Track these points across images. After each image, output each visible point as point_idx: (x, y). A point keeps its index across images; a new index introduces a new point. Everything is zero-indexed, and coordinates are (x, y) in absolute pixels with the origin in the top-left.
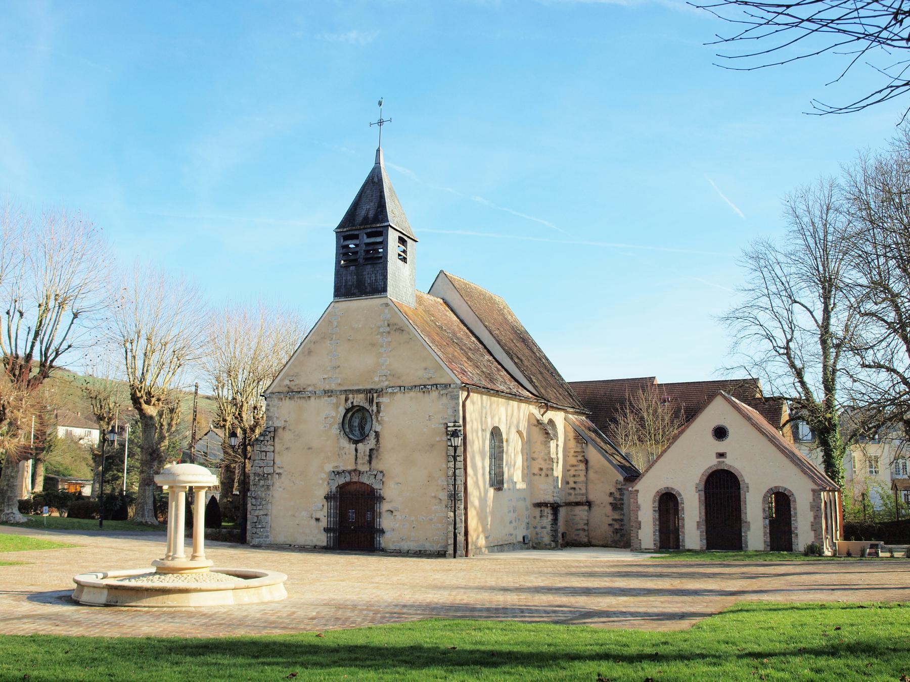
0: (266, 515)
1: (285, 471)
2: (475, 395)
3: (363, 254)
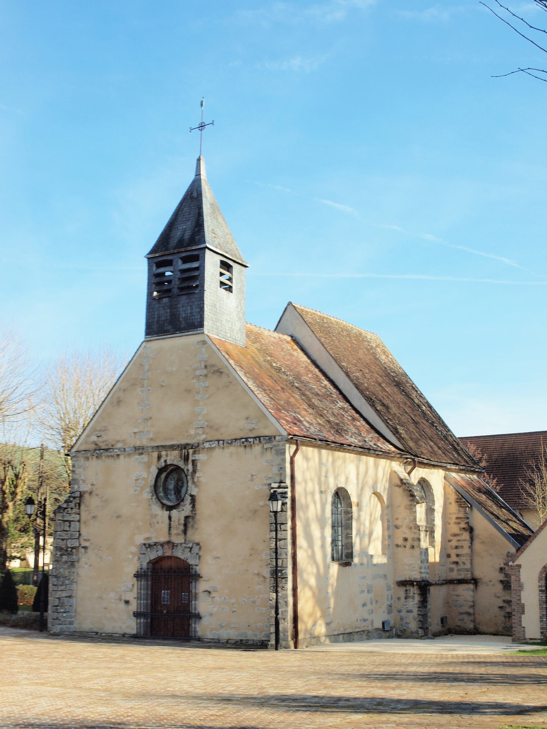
0: (70, 597)
1: (92, 544)
2: (310, 449)
3: (178, 282)
